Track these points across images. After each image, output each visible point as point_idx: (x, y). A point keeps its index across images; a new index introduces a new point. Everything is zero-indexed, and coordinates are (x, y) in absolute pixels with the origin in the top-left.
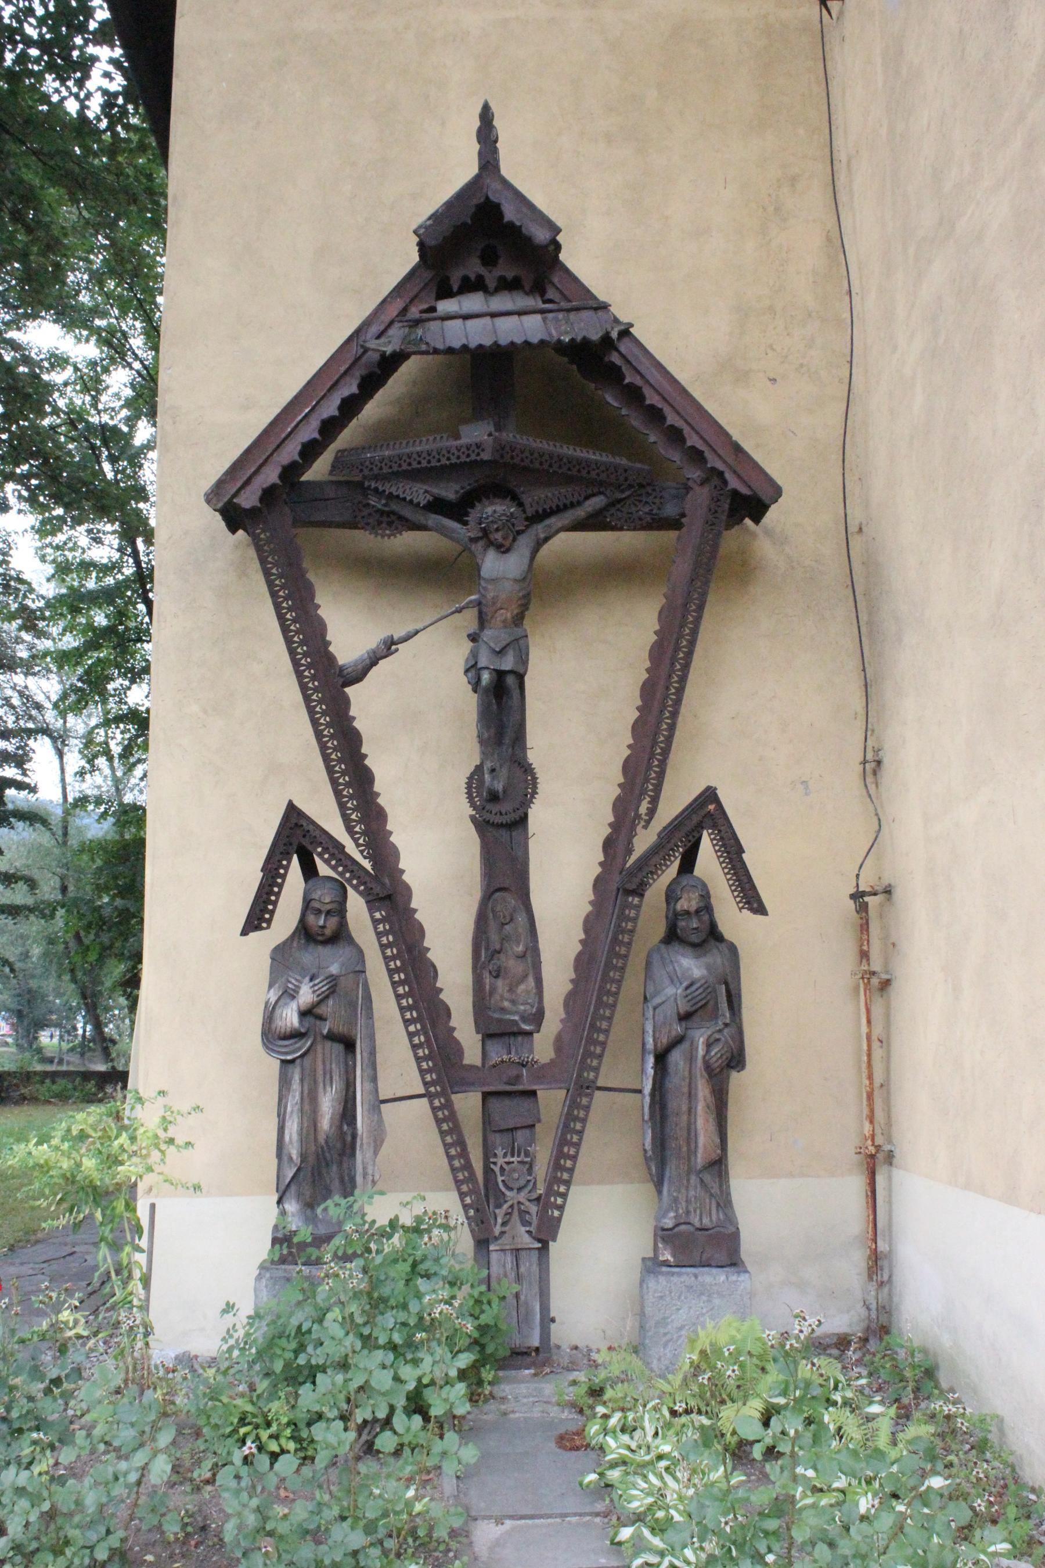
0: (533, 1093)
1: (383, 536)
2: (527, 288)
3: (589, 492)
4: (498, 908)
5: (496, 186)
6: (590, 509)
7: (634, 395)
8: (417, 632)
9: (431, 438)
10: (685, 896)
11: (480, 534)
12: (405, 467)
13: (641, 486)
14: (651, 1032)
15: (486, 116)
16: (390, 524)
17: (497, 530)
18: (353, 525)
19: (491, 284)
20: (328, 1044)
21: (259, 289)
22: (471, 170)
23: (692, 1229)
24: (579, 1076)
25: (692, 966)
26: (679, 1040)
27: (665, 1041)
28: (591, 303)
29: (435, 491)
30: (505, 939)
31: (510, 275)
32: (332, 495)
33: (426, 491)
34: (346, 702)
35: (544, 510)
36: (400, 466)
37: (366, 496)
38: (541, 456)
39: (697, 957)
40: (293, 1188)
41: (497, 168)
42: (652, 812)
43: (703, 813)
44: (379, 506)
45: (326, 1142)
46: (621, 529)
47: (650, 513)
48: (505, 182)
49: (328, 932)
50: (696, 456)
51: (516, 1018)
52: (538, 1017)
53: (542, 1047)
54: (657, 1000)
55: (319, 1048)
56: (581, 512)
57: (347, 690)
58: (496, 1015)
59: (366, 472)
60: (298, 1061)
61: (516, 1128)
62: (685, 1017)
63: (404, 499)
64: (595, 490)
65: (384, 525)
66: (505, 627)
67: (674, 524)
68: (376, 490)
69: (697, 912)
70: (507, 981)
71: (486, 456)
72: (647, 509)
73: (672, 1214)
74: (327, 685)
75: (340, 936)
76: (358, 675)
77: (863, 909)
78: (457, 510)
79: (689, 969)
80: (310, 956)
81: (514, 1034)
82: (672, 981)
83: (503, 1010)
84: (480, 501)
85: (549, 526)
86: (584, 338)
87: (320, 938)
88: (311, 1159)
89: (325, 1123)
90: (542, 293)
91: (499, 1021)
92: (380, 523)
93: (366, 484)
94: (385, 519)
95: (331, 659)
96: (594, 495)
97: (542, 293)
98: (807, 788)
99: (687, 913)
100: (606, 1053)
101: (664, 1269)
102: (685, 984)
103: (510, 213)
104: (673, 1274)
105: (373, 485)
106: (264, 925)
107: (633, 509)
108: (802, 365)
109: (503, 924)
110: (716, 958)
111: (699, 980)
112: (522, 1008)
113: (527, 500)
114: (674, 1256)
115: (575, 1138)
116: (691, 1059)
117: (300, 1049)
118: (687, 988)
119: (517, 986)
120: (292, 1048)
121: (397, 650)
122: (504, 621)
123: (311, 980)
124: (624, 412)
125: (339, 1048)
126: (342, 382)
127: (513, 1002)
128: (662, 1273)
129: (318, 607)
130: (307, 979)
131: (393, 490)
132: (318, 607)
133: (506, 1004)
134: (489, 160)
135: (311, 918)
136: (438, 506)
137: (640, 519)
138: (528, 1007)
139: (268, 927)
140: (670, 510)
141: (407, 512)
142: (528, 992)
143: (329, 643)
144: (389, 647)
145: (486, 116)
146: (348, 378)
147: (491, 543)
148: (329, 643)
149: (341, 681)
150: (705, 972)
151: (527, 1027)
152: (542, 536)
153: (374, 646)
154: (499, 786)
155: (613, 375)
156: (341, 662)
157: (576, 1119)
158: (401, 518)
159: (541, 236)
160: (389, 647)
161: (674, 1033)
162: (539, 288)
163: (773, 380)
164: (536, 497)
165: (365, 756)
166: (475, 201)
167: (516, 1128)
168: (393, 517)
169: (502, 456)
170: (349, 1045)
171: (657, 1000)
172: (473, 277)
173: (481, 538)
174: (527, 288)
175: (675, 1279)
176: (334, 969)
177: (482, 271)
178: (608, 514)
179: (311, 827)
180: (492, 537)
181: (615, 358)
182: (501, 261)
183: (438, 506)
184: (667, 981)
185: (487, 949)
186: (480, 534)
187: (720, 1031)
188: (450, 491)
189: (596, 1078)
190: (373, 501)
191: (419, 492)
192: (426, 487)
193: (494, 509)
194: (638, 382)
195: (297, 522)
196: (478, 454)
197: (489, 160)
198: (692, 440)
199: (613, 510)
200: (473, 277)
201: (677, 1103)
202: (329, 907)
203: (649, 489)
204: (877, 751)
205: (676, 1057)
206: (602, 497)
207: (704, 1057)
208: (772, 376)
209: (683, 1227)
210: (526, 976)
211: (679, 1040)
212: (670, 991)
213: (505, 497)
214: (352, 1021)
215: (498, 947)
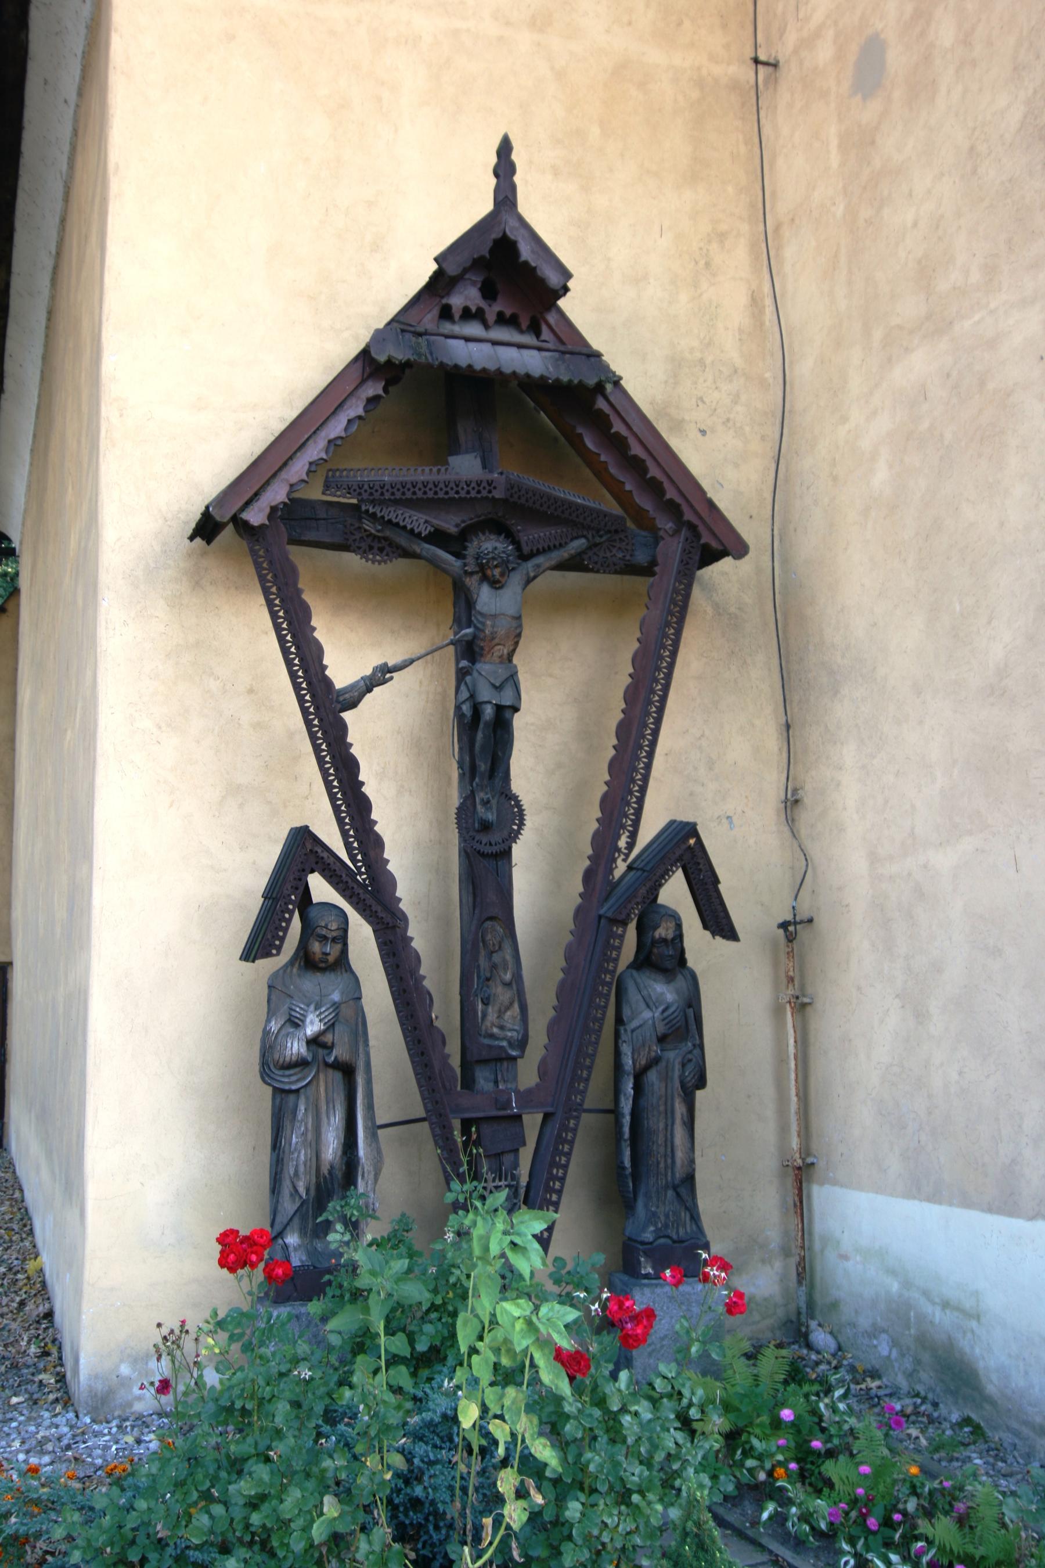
0: (518, 1118)
1: (373, 562)
2: (524, 326)
3: (575, 535)
4: (489, 937)
5: (512, 223)
6: (573, 552)
7: (618, 444)
8: (411, 662)
9: (435, 470)
10: (663, 925)
11: (477, 569)
12: (409, 495)
13: (616, 531)
14: (629, 1054)
15: (505, 149)
16: (381, 550)
17: (496, 566)
18: (343, 547)
19: (491, 317)
20: (330, 1071)
21: (218, 298)
22: (485, 206)
23: (669, 1241)
24: (569, 1099)
25: (664, 992)
26: (655, 1061)
27: (643, 1062)
28: (585, 350)
29: (435, 522)
30: (494, 967)
31: (508, 313)
32: (323, 515)
33: (426, 522)
34: (343, 728)
35: (538, 550)
36: (403, 494)
37: (360, 519)
38: (382, 488)
39: (669, 982)
40: (296, 1220)
41: (513, 204)
42: (631, 846)
43: (683, 847)
44: (373, 531)
45: (330, 1173)
46: (598, 572)
47: (623, 559)
48: (521, 219)
49: (331, 959)
50: (673, 509)
51: (504, 1044)
52: (522, 1043)
53: (527, 1073)
54: (634, 1024)
55: (322, 1076)
56: (564, 554)
57: (343, 715)
58: (486, 1041)
59: (365, 496)
60: (302, 1091)
61: (503, 1153)
62: (662, 1039)
63: (405, 527)
64: (580, 533)
65: (375, 551)
66: (501, 663)
67: (647, 570)
68: (367, 511)
69: (673, 939)
70: (496, 1008)
71: (498, 494)
72: (620, 555)
73: (652, 1228)
74: (325, 709)
75: (341, 963)
76: (352, 698)
77: (790, 939)
78: (454, 543)
79: (662, 994)
80: (310, 983)
81: (500, 1060)
82: (648, 1006)
83: (492, 1036)
84: (477, 536)
85: (538, 566)
86: (580, 382)
87: (323, 965)
88: (313, 1192)
89: (669, 1178)
90: (538, 334)
91: (490, 1047)
92: (371, 548)
93: (364, 508)
94: (376, 545)
95: (328, 683)
96: (577, 538)
97: (538, 334)
98: (731, 823)
99: (664, 941)
100: (593, 1076)
101: (646, 1281)
102: (661, 1009)
103: (526, 252)
104: (656, 1285)
105: (371, 510)
106: (274, 952)
107: (608, 554)
108: (728, 420)
109: (492, 952)
110: (680, 982)
111: (673, 1003)
112: (509, 1034)
113: (523, 538)
114: (653, 1268)
115: (563, 1160)
116: (666, 1078)
117: (304, 1078)
118: (664, 1011)
119: (505, 1011)
120: (299, 1076)
121: (391, 678)
122: (501, 657)
123: (316, 1009)
124: (603, 458)
125: (338, 1076)
126: (348, 403)
127: (502, 1028)
128: (645, 1285)
129: (314, 629)
130: (312, 1007)
131: (392, 516)
132: (314, 629)
133: (495, 1030)
134: (506, 195)
135: (316, 947)
136: (438, 538)
137: (615, 565)
138: (515, 1034)
139: (278, 954)
140: (641, 557)
141: (402, 541)
142: (514, 1018)
143: (326, 667)
144: (381, 676)
145: (505, 149)
146: (354, 400)
147: (485, 578)
148: (326, 667)
149: (339, 706)
150: (676, 997)
151: (514, 1053)
152: (532, 574)
153: (368, 672)
154: (491, 817)
155: (600, 423)
156: (337, 687)
157: (565, 1141)
158: (391, 543)
159: (553, 279)
160: (381, 676)
161: (653, 1054)
162: (535, 329)
163: (703, 432)
164: (531, 535)
165: (362, 784)
166: (494, 236)
167: (503, 1153)
168: (384, 543)
169: (511, 496)
170: (347, 1071)
171: (634, 1024)
172: (474, 309)
173: (477, 572)
174: (524, 326)
175: (658, 1290)
176: (336, 997)
177: (483, 304)
178: (585, 557)
179: (325, 855)
180: (489, 572)
181: (601, 404)
182: (499, 297)
183: (438, 538)
184: (643, 1005)
185: (479, 977)
186: (477, 569)
187: (690, 1052)
188: (450, 523)
189: (583, 1101)
190: (368, 525)
191: (418, 521)
192: (425, 517)
193: (490, 545)
194: (624, 431)
195: (293, 541)
196: (490, 492)
197: (506, 195)
198: (671, 494)
199: (590, 553)
200: (474, 309)
201: (655, 1122)
202: (334, 934)
203: (622, 536)
204: (795, 791)
205: (652, 1076)
206: (583, 541)
207: (680, 1077)
208: (703, 427)
209: (662, 1241)
210: (511, 1004)
211: (655, 1061)
212: (647, 1014)
213: (500, 534)
214: (355, 1051)
215: (488, 975)
